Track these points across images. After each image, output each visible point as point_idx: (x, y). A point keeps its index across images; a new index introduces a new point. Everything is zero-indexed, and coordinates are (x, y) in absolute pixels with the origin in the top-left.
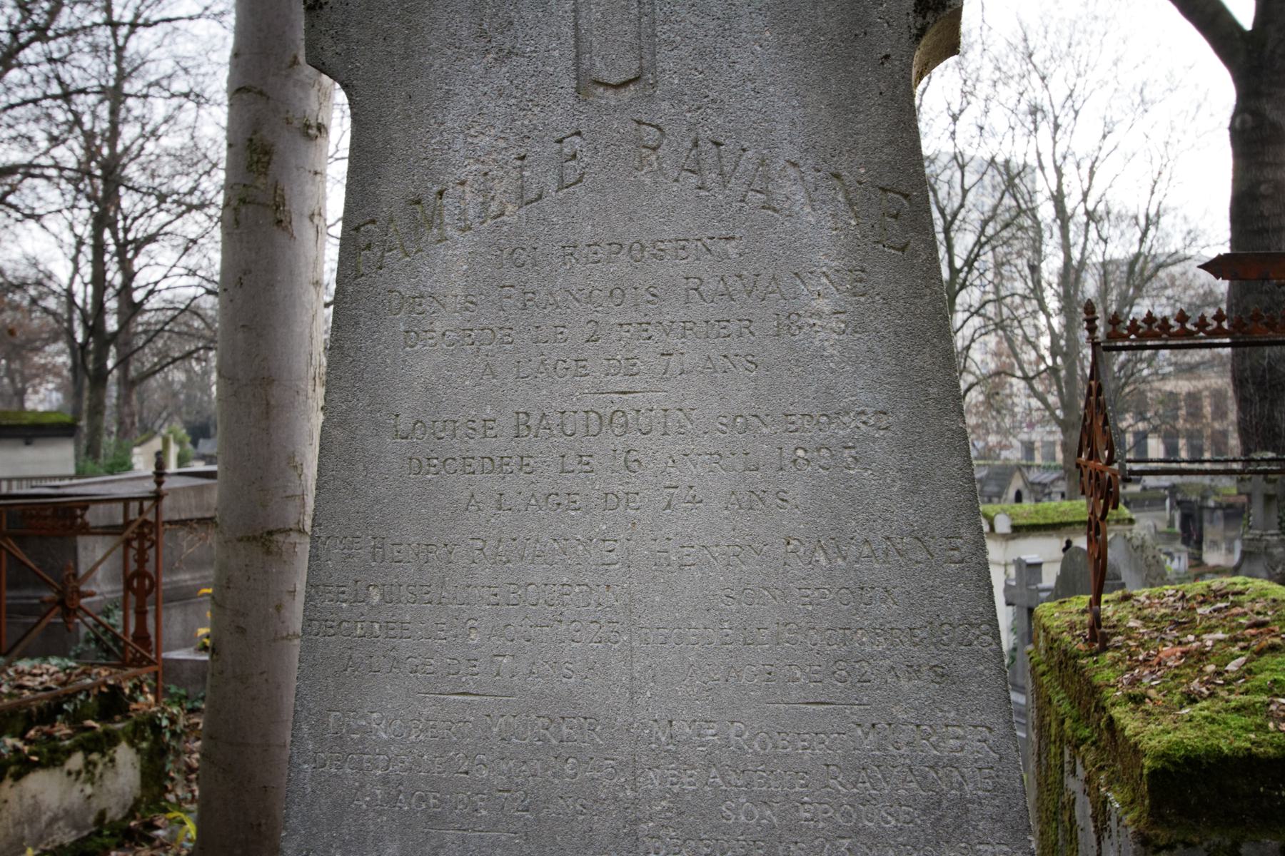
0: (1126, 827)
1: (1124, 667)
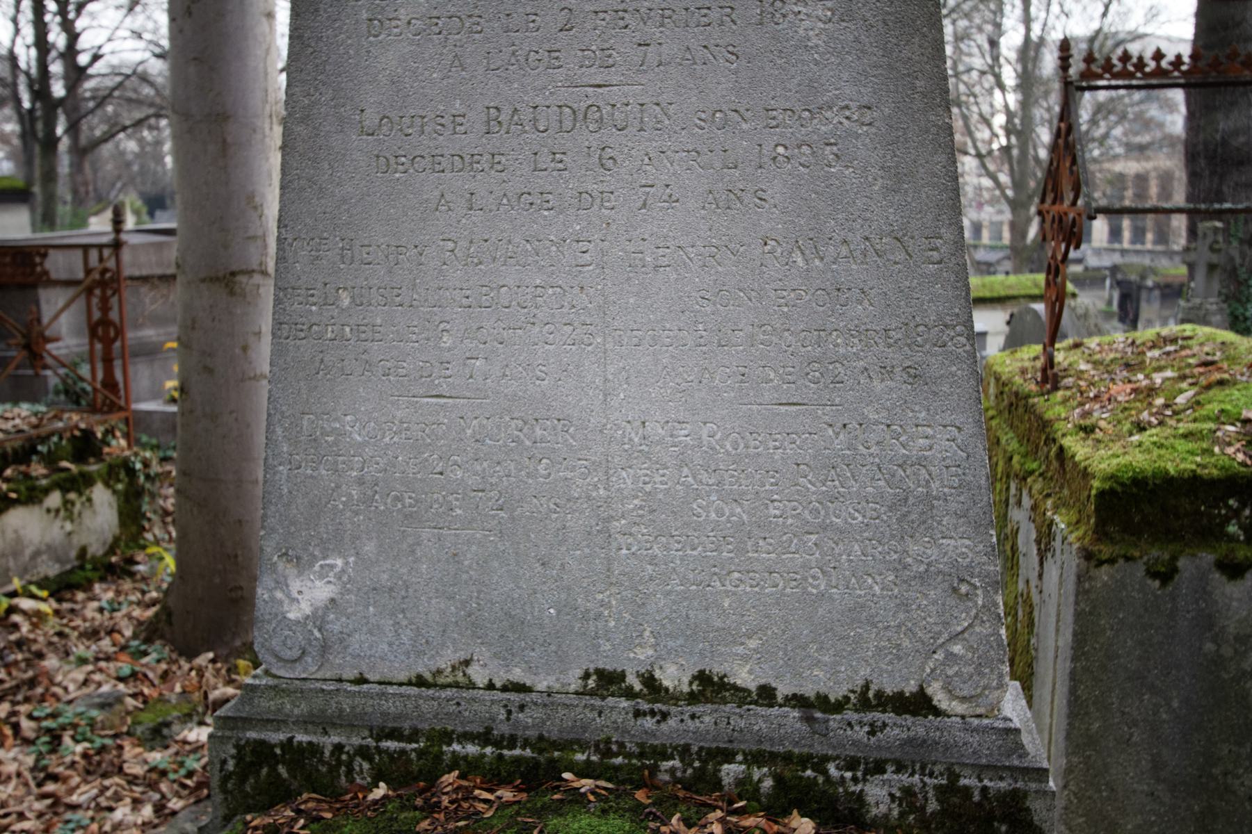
0: (1071, 544)
1: (1075, 403)
